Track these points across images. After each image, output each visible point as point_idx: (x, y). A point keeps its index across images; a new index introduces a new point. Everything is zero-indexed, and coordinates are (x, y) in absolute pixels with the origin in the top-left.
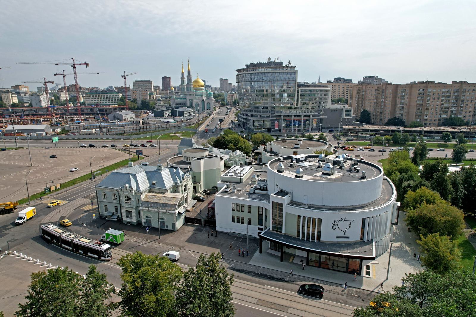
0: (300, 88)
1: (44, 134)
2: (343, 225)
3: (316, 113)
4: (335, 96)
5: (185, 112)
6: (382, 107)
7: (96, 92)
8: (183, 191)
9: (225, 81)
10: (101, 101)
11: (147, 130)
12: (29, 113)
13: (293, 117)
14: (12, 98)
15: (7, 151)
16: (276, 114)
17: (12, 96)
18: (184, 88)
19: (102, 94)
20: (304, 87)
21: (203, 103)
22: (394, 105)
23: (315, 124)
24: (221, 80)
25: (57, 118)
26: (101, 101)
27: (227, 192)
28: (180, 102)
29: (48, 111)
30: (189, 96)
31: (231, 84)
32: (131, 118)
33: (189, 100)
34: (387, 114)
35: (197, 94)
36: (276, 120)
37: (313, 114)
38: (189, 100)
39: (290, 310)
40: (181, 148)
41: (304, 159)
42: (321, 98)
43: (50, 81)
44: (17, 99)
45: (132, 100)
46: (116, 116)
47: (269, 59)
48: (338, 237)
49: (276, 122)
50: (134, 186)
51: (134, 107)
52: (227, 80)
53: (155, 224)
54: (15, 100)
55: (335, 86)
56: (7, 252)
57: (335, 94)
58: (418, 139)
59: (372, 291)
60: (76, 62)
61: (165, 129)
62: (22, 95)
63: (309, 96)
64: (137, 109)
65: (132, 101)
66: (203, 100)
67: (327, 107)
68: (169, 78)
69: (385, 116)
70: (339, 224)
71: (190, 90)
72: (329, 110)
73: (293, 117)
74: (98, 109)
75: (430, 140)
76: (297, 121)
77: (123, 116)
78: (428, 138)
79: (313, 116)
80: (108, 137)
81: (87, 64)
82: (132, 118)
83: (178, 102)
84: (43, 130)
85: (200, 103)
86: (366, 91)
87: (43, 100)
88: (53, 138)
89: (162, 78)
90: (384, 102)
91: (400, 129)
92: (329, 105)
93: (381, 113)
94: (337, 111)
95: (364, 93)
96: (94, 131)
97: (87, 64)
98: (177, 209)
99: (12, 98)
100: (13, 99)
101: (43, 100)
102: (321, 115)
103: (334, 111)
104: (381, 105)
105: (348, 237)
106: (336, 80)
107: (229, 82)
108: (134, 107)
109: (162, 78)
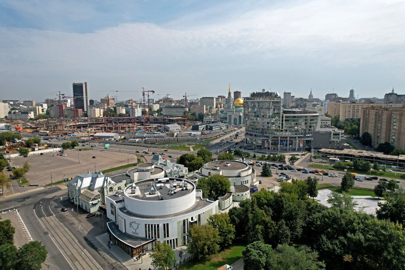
0: (284, 115)
1: (113, 139)
2: (135, 226)
3: (301, 136)
4: (357, 116)
5: (214, 127)
6: (379, 131)
7: (170, 107)
8: (108, 191)
9: (288, 94)
10: (173, 114)
11: (172, 141)
12: (126, 121)
13: (288, 138)
14: (122, 110)
15: (82, 151)
16: (265, 135)
17: (122, 109)
18: (230, 106)
19: (173, 108)
20: (292, 113)
21: (240, 118)
22: (389, 130)
23: (301, 145)
24: (285, 93)
25: (138, 126)
26: (173, 114)
27: (116, 195)
28: (223, 117)
29: (138, 119)
30: (228, 112)
31: (293, 96)
32: (177, 129)
33: (229, 115)
34: (383, 139)
35: (237, 111)
36: (265, 140)
37: (298, 136)
38: (229, 115)
39: (76, 263)
40: (154, 161)
41: (166, 181)
42: (307, 123)
43: (148, 97)
44: (125, 110)
45: (192, 113)
46: (166, 128)
47: (264, 90)
48: (133, 233)
49: (266, 141)
50: (79, 185)
51: (193, 119)
52: (290, 93)
53: (84, 208)
54: (124, 111)
55: (357, 106)
56: (14, 209)
57: (357, 114)
58: (386, 167)
59: (124, 266)
60: (145, 90)
61: (185, 141)
62: (129, 107)
63: (293, 121)
64: (195, 120)
65: (192, 114)
66: (240, 116)
67: (317, 130)
68: (239, 92)
69: (381, 140)
70: (133, 224)
71: (230, 108)
72: (318, 132)
73: (288, 138)
74: (168, 119)
75: (400, 169)
76: (285, 141)
77: (170, 128)
78: (397, 168)
79: (299, 137)
80: (146, 145)
81: (153, 92)
82: (178, 129)
83: (221, 117)
84: (112, 137)
85: (238, 118)
86: (369, 115)
87: (136, 112)
88: (106, 145)
89: (234, 92)
90: (381, 127)
91: (373, 155)
92: (318, 129)
93: (378, 137)
94: (325, 134)
95: (367, 117)
96: (137, 140)
97: (153, 92)
98: (91, 201)
99: (122, 110)
100: (123, 110)
101: (136, 112)
102: (308, 137)
103: (323, 134)
104: (378, 129)
105: (138, 234)
106: (387, 95)
107: (292, 95)
108: (193, 119)
109: (234, 92)
